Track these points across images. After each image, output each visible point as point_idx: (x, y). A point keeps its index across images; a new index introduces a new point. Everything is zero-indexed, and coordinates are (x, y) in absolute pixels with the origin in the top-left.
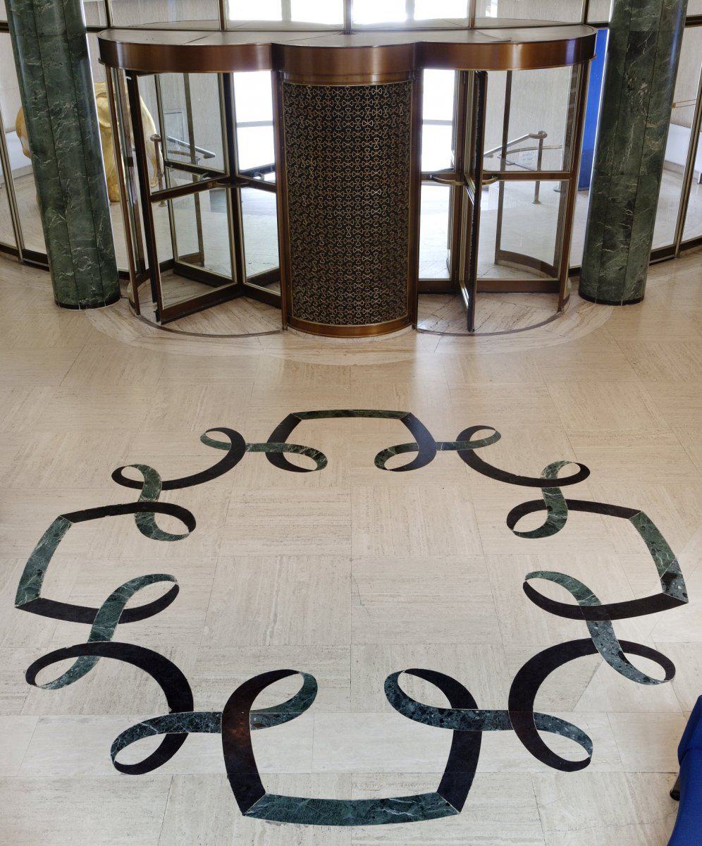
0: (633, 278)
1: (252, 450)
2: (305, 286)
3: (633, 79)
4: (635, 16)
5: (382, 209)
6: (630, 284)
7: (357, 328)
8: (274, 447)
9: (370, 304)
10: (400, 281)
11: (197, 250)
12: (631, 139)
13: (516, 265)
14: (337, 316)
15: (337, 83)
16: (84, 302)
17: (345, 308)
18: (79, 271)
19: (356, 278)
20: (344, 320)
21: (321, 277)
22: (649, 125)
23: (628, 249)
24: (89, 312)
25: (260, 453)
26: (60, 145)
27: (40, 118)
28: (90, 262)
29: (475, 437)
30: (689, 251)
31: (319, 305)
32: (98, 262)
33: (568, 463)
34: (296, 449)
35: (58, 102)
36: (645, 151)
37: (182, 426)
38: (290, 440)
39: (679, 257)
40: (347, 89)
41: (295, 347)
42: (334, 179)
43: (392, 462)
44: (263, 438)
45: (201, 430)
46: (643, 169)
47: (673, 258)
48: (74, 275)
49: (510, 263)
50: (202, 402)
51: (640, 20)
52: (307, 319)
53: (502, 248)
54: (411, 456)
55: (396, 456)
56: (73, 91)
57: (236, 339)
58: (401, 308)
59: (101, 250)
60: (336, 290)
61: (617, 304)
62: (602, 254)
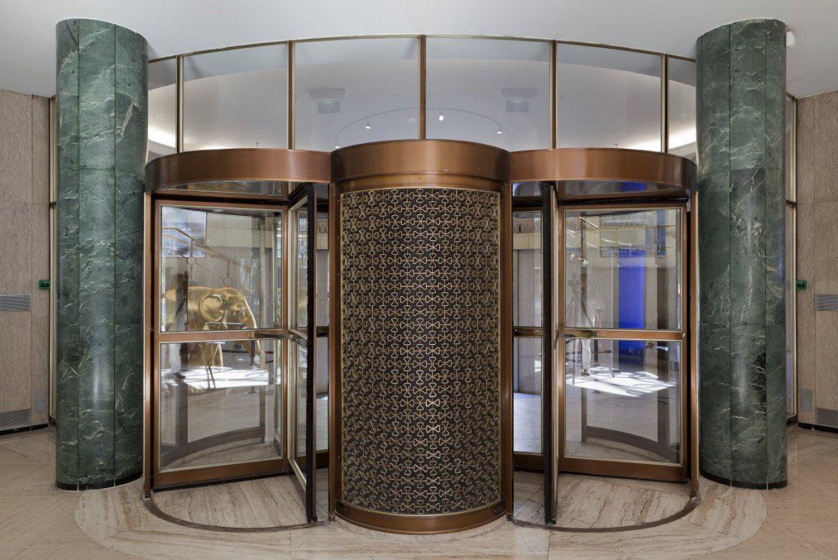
0: (776, 453)
2: (359, 455)
3: (743, 219)
4: (735, 154)
5: (454, 438)
6: (774, 461)
7: (431, 519)
9: (449, 482)
10: (482, 464)
11: (254, 422)
12: (750, 285)
13: (607, 443)
14: (402, 500)
16: (84, 480)
17: (414, 488)
18: (84, 439)
19: (429, 444)
20: (412, 507)
21: (381, 442)
22: (769, 268)
23: (766, 415)
26: (86, 286)
27: (68, 256)
28: (102, 429)
31: (378, 484)
36: (769, 298)
41: (340, 548)
42: (401, 306)
48: (78, 445)
49: (600, 441)
51: (742, 158)
52: (361, 504)
56: (113, 229)
57: (263, 534)
60: (401, 461)
62: (731, 423)
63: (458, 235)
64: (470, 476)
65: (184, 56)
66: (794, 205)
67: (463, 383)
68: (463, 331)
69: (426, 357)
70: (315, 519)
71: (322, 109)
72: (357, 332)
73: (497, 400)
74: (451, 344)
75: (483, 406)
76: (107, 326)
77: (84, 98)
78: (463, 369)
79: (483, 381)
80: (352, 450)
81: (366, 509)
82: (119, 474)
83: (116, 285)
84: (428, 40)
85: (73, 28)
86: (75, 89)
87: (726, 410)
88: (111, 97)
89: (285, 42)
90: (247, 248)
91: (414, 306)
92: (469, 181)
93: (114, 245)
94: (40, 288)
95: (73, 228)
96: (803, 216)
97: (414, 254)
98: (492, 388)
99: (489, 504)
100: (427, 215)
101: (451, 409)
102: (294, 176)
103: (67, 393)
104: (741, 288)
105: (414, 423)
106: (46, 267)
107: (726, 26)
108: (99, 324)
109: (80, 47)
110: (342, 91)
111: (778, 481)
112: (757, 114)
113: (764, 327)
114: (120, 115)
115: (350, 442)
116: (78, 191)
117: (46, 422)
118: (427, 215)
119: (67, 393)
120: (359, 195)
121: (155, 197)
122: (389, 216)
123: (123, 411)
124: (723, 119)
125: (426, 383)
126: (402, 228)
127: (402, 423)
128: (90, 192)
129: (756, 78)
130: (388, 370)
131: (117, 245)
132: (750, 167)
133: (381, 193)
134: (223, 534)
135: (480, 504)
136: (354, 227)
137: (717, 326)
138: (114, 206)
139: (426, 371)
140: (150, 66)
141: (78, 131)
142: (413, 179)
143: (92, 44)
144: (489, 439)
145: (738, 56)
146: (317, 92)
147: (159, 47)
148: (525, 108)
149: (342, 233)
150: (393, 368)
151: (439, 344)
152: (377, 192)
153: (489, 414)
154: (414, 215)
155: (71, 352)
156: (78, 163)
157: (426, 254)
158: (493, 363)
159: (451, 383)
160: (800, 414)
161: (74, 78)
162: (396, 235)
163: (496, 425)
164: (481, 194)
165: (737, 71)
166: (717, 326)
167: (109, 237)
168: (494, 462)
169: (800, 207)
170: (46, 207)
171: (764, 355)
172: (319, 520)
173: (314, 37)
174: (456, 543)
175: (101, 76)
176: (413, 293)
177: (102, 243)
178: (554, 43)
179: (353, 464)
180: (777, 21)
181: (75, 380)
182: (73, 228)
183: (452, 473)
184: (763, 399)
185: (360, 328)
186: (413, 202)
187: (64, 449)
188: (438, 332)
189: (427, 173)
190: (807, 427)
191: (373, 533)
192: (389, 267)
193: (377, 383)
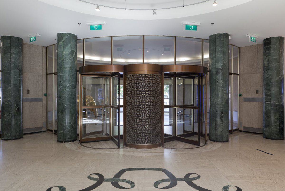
1: (106, 181)
3: (218, 80)
4: (217, 65)
8: (115, 180)
11: (101, 130)
15: (141, 73)
16: (65, 140)
17: (142, 139)
18: (65, 131)
22: (224, 91)
24: (66, 143)
25: (109, 182)
29: (191, 177)
30: (235, 132)
32: (71, 128)
33: (231, 186)
34: (123, 180)
35: (62, 74)
36: (224, 98)
37: (82, 173)
38: (121, 178)
39: (233, 133)
40: (144, 75)
42: (139, 99)
43: (160, 186)
44: (111, 177)
45: (88, 174)
46: (224, 103)
47: (231, 134)
48: (63, 132)
50: (92, 166)
51: (218, 65)
52: (130, 143)
53: (185, 130)
54: (168, 183)
55: (162, 183)
56: (71, 82)
58: (159, 140)
59: (72, 125)
61: (222, 142)
63: (152, 84)
64: (154, 137)
65: (85, 39)
66: (239, 75)
67: (153, 116)
68: (153, 105)
69: (145, 111)
70: (120, 147)
71: (118, 50)
72: (129, 105)
73: (160, 121)
74: (150, 108)
75: (157, 121)
76: (70, 104)
77: (64, 51)
78: (153, 113)
79: (157, 116)
80: (128, 131)
81: (132, 144)
82: (72, 139)
83: (71, 95)
84: (145, 36)
85: (62, 35)
86: (62, 49)
87: (215, 124)
88: (70, 51)
89: (111, 37)
90: (90, 84)
91: (142, 99)
92: (154, 72)
93: (71, 85)
94: (44, 96)
95: (62, 82)
96: (241, 77)
97: (142, 88)
98: (159, 118)
99: (158, 143)
100: (145, 80)
101: (150, 122)
102: (114, 70)
103: (60, 121)
104: (217, 96)
105: (139, 139)
106: (46, 90)
107: (215, 34)
108: (67, 104)
109: (64, 39)
110: (123, 45)
111: (226, 140)
112: (222, 55)
113: (223, 105)
114: (72, 55)
115: (128, 129)
116: (63, 73)
117: (46, 130)
118: (145, 80)
119: (60, 121)
120: (130, 75)
121: (82, 74)
122: (137, 80)
123: (73, 124)
124: (214, 56)
125: (145, 116)
126: (139, 83)
127: (139, 125)
128: (66, 73)
129: (222, 47)
130: (137, 113)
131: (72, 86)
132: (220, 68)
133: (135, 75)
134: (101, 149)
135: (157, 143)
136: (129, 82)
137: (213, 105)
138: (71, 76)
139: (145, 114)
140: (78, 40)
141: (63, 59)
142: (142, 72)
143: (66, 39)
144: (159, 129)
145: (218, 41)
146: (117, 46)
147: (79, 37)
148: (169, 50)
149: (126, 83)
150: (138, 113)
151: (148, 108)
152: (134, 75)
153: (159, 123)
154: (142, 80)
155: (61, 110)
156: (63, 66)
157: (145, 88)
158: (159, 112)
159: (150, 116)
160: (240, 128)
161: (62, 47)
162: (138, 84)
163: (160, 126)
164: (157, 75)
165: (217, 45)
166: (213, 105)
167: (70, 84)
168: (160, 134)
169: (240, 75)
170: (46, 75)
171: (223, 111)
172: (121, 147)
173: (118, 36)
174: (151, 151)
175: (68, 46)
176: (142, 97)
177: (69, 85)
178: (175, 37)
179: (129, 134)
180: (226, 34)
181: (63, 117)
182: (62, 82)
183: (150, 136)
184: (223, 121)
185: (130, 105)
186: (142, 77)
187: (60, 133)
188: (147, 105)
189: (145, 71)
190: (241, 131)
191: (133, 149)
192: (137, 91)
193: (134, 116)
